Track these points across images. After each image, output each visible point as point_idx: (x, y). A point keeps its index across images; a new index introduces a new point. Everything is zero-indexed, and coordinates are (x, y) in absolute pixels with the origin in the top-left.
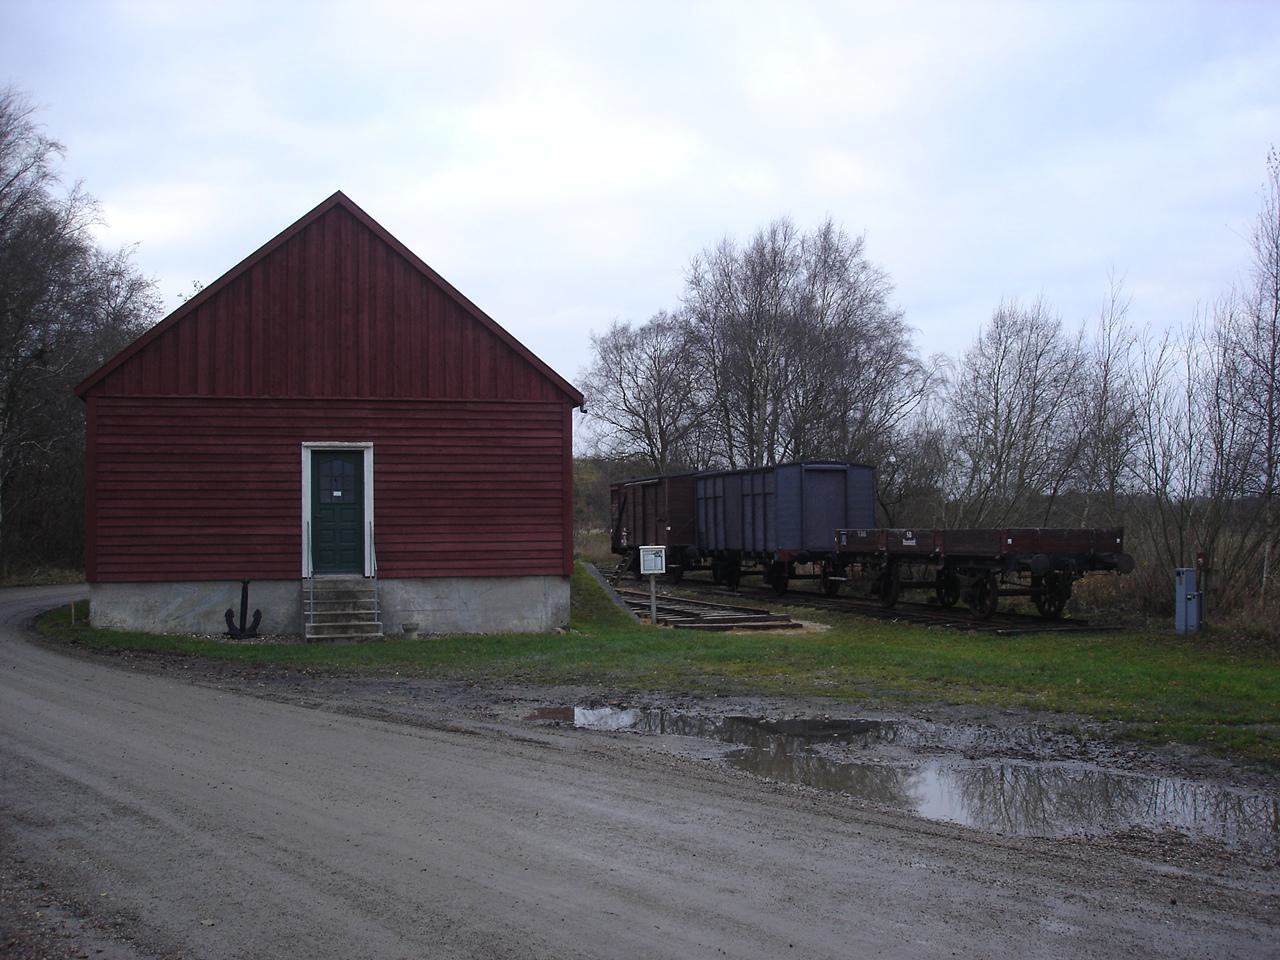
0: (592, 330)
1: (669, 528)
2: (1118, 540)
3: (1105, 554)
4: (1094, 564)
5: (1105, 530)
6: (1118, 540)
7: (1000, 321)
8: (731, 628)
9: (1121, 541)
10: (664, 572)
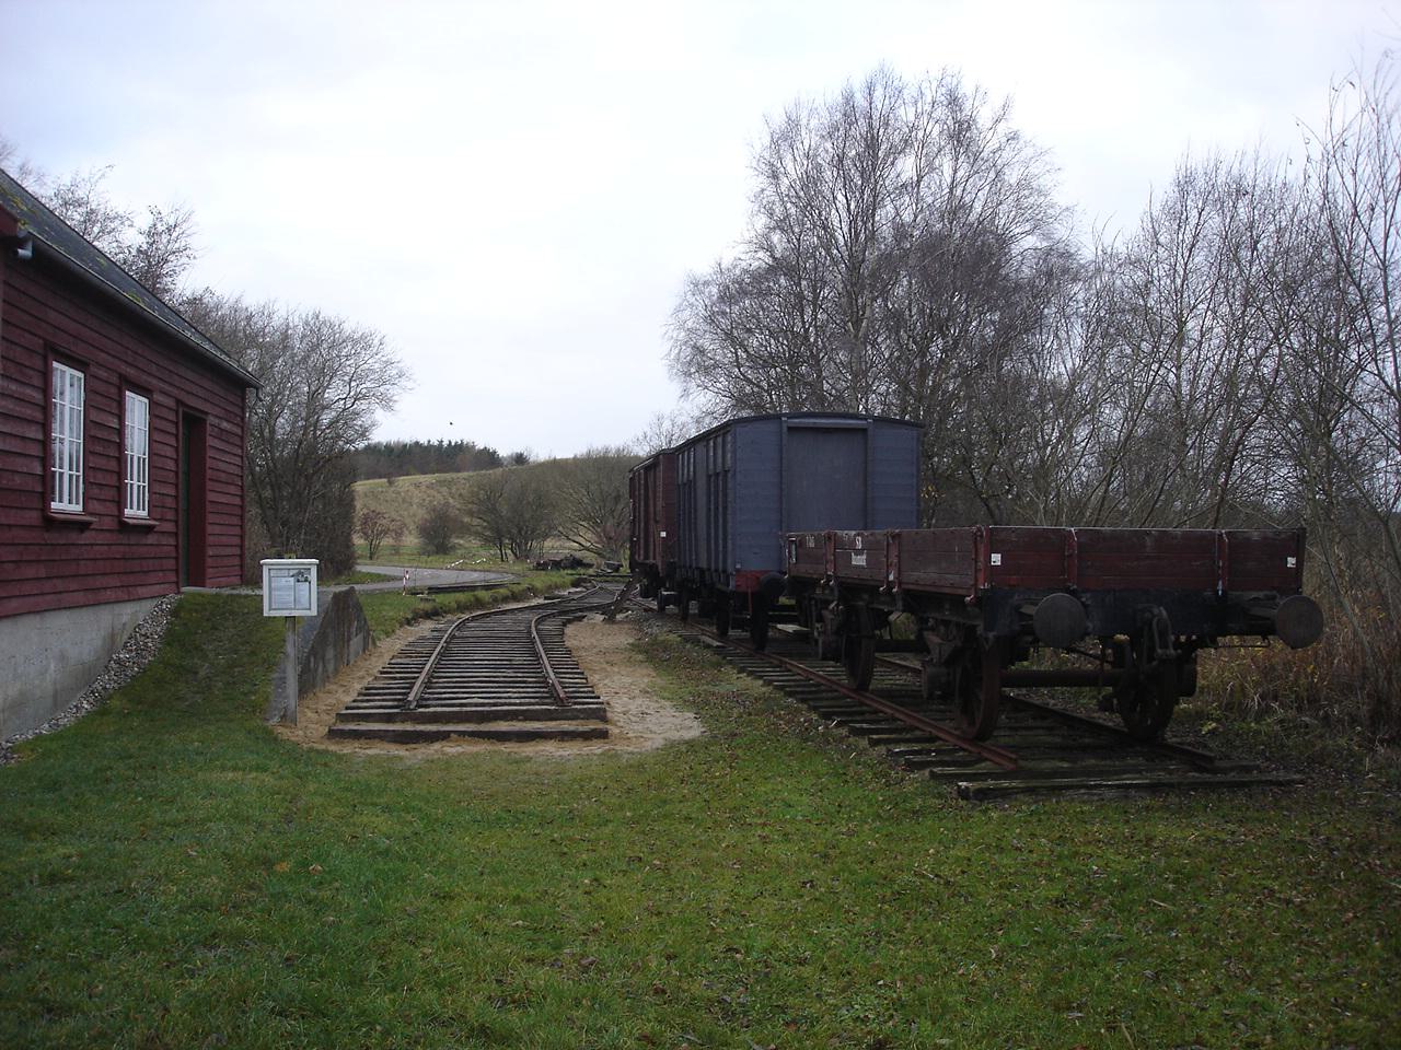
0: (721, 259)
1: (663, 534)
2: (1291, 561)
3: (1254, 595)
4: (1224, 618)
5: (1256, 536)
6: (1291, 561)
7: (1184, 185)
8: (444, 736)
9: (1300, 563)
10: (315, 613)
